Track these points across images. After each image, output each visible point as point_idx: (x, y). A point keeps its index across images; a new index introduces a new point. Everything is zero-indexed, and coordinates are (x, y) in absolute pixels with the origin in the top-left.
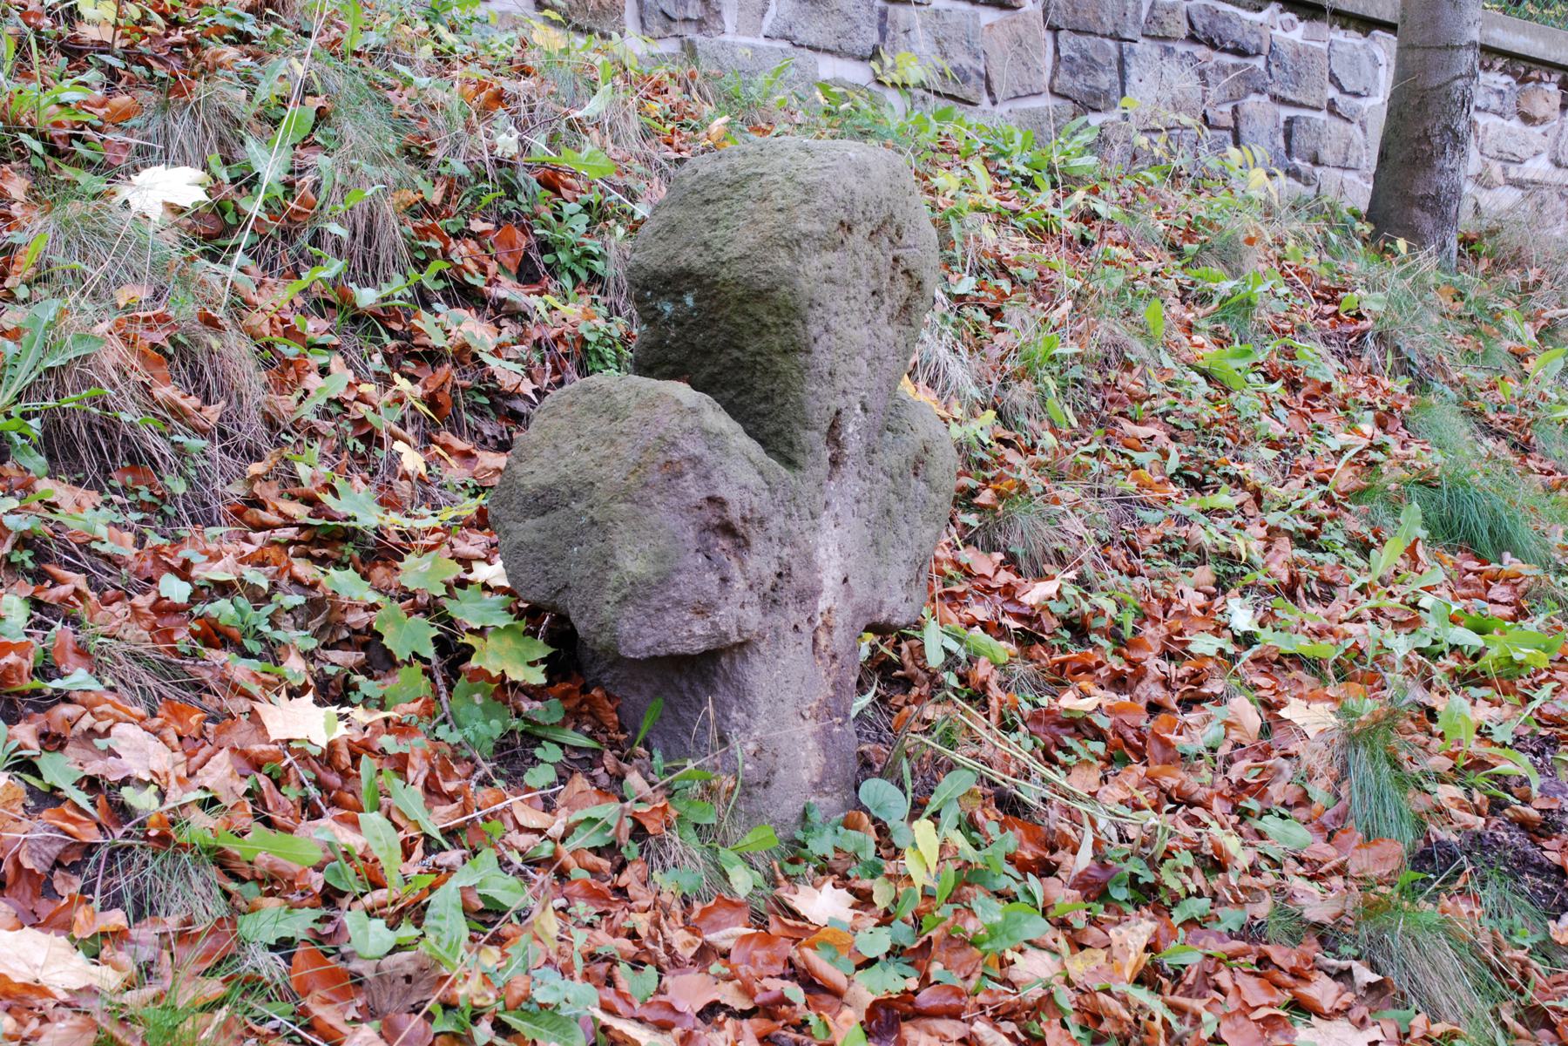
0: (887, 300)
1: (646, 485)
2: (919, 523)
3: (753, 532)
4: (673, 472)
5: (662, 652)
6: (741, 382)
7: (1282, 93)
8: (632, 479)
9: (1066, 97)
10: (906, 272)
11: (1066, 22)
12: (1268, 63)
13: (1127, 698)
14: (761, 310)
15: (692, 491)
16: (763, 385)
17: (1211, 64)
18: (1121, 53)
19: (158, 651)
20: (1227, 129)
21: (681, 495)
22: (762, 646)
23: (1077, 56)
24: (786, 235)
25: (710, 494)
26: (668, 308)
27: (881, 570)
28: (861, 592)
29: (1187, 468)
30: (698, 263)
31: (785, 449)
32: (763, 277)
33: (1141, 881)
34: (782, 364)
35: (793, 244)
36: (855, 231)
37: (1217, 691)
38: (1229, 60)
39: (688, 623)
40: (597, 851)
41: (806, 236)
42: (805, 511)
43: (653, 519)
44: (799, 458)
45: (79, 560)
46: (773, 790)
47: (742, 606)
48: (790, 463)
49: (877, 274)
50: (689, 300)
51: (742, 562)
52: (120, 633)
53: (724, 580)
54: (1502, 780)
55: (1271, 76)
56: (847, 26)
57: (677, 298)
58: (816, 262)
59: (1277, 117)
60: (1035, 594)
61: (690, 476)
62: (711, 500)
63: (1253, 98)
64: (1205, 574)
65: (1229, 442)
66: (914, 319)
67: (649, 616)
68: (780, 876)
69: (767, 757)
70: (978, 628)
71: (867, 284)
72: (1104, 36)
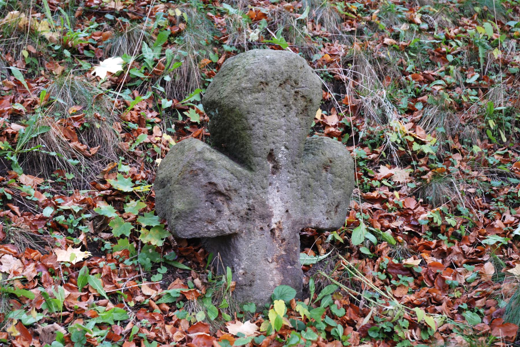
0: (294, 108)
1: (184, 178)
3: (232, 194)
4: (194, 174)
5: (198, 236)
8: (180, 176)
10: (303, 96)
15: (202, 180)
19: (31, 232)
21: (199, 182)
22: (243, 235)
24: (238, 89)
25: (210, 181)
26: (213, 114)
28: (296, 215)
30: (216, 99)
31: (249, 164)
32: (231, 103)
33: (385, 331)
35: (240, 92)
36: (270, 85)
39: (206, 226)
40: (167, 304)
41: (244, 89)
42: (258, 186)
43: (188, 190)
44: (253, 167)
45: (23, 202)
46: (254, 288)
47: (230, 220)
48: (251, 169)
52: (19, 226)
53: (219, 211)
61: (201, 175)
62: (210, 183)
66: (309, 114)
67: (189, 224)
69: (249, 275)
70: (390, 230)
71: (280, 103)
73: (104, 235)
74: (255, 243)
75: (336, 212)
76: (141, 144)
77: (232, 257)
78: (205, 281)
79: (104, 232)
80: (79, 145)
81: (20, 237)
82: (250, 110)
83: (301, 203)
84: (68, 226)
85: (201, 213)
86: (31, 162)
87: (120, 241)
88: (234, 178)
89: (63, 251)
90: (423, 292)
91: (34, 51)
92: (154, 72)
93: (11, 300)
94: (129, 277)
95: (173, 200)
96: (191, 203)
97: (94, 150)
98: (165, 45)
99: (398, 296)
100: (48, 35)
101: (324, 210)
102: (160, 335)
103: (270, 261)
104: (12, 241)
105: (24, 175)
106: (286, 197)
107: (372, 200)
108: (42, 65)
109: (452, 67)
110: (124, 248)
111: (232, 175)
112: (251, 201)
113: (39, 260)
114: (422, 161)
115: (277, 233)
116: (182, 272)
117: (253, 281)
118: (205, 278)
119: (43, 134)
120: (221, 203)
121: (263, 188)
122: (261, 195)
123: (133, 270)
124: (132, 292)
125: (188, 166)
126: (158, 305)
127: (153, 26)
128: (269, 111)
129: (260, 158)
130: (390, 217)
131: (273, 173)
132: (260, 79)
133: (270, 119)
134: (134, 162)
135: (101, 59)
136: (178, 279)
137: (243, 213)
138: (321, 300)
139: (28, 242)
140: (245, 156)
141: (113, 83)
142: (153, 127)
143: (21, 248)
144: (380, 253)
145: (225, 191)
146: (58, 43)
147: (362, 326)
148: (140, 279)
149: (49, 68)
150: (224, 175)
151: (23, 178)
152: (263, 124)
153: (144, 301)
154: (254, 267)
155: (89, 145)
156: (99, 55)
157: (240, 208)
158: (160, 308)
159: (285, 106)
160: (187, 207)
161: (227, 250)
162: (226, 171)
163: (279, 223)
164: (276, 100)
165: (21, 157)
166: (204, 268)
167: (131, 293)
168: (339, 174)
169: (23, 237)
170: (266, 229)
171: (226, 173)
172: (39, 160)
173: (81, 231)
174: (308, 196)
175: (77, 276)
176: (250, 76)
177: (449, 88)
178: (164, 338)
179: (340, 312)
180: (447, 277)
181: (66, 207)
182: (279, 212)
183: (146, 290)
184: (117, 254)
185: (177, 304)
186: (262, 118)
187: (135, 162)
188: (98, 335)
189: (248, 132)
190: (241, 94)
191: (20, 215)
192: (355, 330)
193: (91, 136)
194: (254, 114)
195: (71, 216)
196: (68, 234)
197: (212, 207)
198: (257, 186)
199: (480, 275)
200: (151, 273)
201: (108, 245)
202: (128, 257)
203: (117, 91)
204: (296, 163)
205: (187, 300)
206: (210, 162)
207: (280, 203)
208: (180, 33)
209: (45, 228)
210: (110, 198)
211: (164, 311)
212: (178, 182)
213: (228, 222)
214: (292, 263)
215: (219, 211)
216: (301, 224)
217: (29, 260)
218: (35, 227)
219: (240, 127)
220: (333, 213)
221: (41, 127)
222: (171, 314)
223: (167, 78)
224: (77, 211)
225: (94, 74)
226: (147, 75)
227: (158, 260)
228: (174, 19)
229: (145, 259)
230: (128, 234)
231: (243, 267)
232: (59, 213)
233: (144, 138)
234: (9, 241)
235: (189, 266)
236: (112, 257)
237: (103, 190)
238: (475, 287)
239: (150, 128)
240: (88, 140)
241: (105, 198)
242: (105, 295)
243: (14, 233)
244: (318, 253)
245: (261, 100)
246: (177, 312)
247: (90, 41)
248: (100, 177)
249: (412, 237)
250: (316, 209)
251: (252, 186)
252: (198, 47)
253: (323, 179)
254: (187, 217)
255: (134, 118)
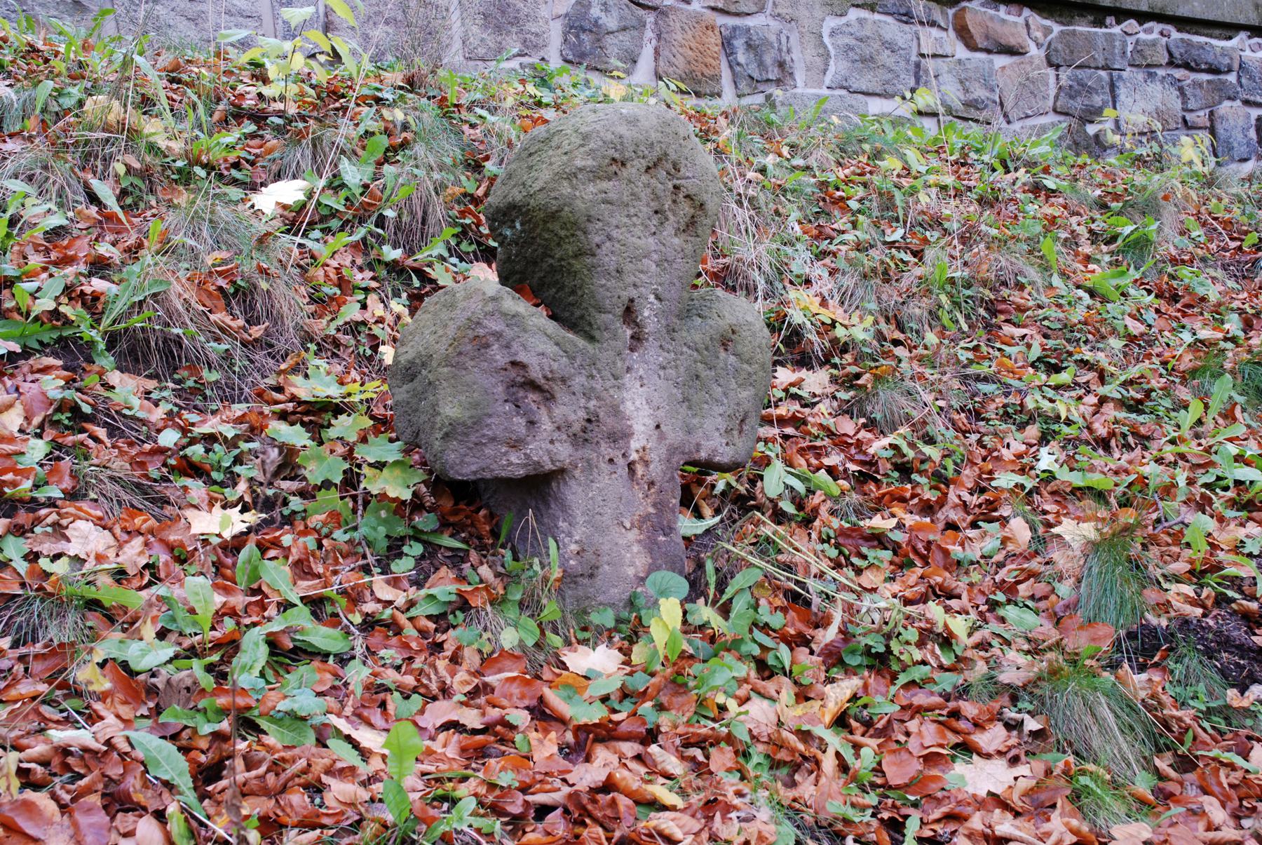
1: (460, 353)
2: (734, 386)
4: (482, 345)
5: (488, 475)
6: (557, 282)
7: (1252, 98)
8: (451, 349)
9: (1067, 114)
10: (687, 196)
11: (1065, 61)
12: (1239, 77)
13: (928, 520)
14: (555, 226)
15: (498, 357)
16: (569, 282)
17: (1188, 82)
18: (1112, 80)
20: (1205, 128)
22: (577, 473)
23: (1075, 84)
26: (508, 233)
27: (695, 421)
28: (674, 435)
29: (1047, 356)
30: (518, 197)
31: (587, 328)
32: (553, 202)
33: (873, 651)
34: (577, 265)
35: (571, 176)
36: (628, 166)
37: (1005, 514)
38: (1205, 77)
39: (505, 454)
40: (429, 617)
41: (580, 170)
42: (606, 373)
43: (469, 378)
44: (597, 334)
46: (598, 581)
47: (552, 442)
48: (591, 339)
49: (657, 198)
50: (518, 225)
51: (550, 410)
53: (532, 423)
54: (1237, 582)
55: (1241, 86)
56: (890, 76)
59: (1248, 116)
61: (496, 347)
62: (514, 363)
63: (1227, 103)
65: (1090, 337)
66: (699, 232)
68: (573, 640)
69: (589, 555)
70: (823, 471)
71: (648, 205)
72: (1097, 68)
73: (286, 485)
74: (600, 490)
75: (741, 432)
76: (346, 323)
77: (555, 518)
78: (500, 569)
79: (284, 479)
80: (228, 320)
81: (110, 487)
82: (592, 213)
83: (683, 410)
84: (212, 466)
85: (496, 426)
86: (132, 351)
87: (321, 495)
88: (562, 353)
89: (203, 513)
90: (913, 575)
91: (137, 165)
93: (89, 614)
94: (346, 566)
95: (438, 400)
96: (476, 405)
97: (257, 331)
98: (379, 164)
99: (869, 587)
100: (162, 143)
101: (723, 427)
102: (425, 681)
103: (628, 525)
104: (93, 495)
105: (118, 373)
106: (656, 399)
107: (782, 421)
109: (861, 217)
110: (330, 508)
112: (592, 404)
113: (151, 531)
114: (848, 357)
115: (640, 470)
116: (450, 554)
117: (597, 568)
118: (499, 563)
119: (155, 295)
120: (534, 406)
121: (616, 378)
122: (612, 392)
123: (351, 551)
124: (354, 594)
125: (469, 328)
126: (410, 619)
127: (355, 134)
128: (626, 220)
129: (610, 316)
130: (815, 448)
131: (632, 350)
132: (612, 152)
133: (628, 236)
134: (334, 355)
135: (263, 185)
136: (444, 570)
137: (576, 427)
138: (730, 600)
139: (126, 497)
140: (578, 313)
143: (111, 509)
144: (815, 511)
145: (543, 381)
146: (180, 157)
147: (826, 645)
148: (366, 570)
149: (167, 198)
150: (541, 348)
151: (115, 377)
152: (617, 246)
153: (382, 613)
154: (597, 538)
155: (247, 321)
157: (572, 417)
158: (415, 627)
159: (656, 212)
160: (468, 414)
161: (541, 507)
162: (545, 339)
163: (644, 449)
164: (639, 199)
165: (112, 340)
166: (493, 546)
167: (354, 597)
168: (747, 356)
169: (118, 488)
170: (621, 462)
171: (545, 343)
172: (149, 348)
173: (239, 476)
174: (695, 398)
175: (234, 564)
176: (592, 145)
177: (859, 247)
178: (434, 687)
179: (777, 620)
180: (950, 547)
181: (206, 429)
182: (643, 428)
183: (385, 592)
184: (316, 520)
185: (451, 617)
186: (615, 233)
187: (337, 356)
188: (1245, 558)
189: (589, 260)
191: (109, 445)
192: (812, 652)
194: (600, 224)
195: (216, 447)
196: (211, 482)
197: (518, 413)
198: (604, 373)
199: (1005, 541)
200: (388, 557)
201: (296, 503)
202: (340, 527)
203: (296, 234)
204: (674, 331)
205: (471, 607)
206: (513, 319)
207: (646, 411)
208: (404, 145)
209: (164, 470)
210: (293, 418)
211: (423, 633)
212: (447, 361)
213: (550, 447)
214: (667, 531)
215: (532, 423)
216: (683, 453)
217: (129, 533)
218: (142, 465)
219: (570, 249)
220: (735, 433)
222: (440, 637)
223: (390, 213)
224: (230, 436)
225: (253, 206)
227: (401, 530)
228: (391, 126)
229: (375, 529)
230: (337, 479)
231: (577, 538)
232: (193, 441)
233: (351, 312)
234: (86, 495)
235: (464, 541)
236: (306, 527)
237: (277, 402)
238: (1001, 565)
239: (361, 297)
241: (283, 416)
242: (298, 602)
243: (96, 478)
244: (699, 515)
245: (612, 196)
246: (451, 632)
247: (243, 154)
248: (271, 381)
249: (864, 482)
250: (709, 424)
251: (595, 372)
252: (442, 167)
253: (721, 365)
254: (466, 435)
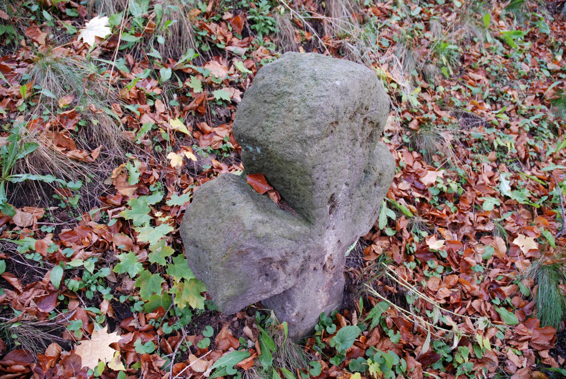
1: (230, 261)
15: (254, 258)
24: (299, 137)
25: (264, 257)
32: (287, 155)
36: (340, 123)
41: (309, 138)
43: (237, 270)
44: (312, 220)
57: (254, 147)
58: (316, 147)
60: (429, 178)
64: (493, 155)
92: (147, 32)
108: (20, 32)
111: (290, 241)
141: (103, 49)
142: (154, 103)
156: (84, 13)
176: (318, 119)
190: (305, 145)
193: (89, 133)
221: (26, 145)
226: (140, 35)
239: (151, 103)
240: (88, 139)
255: (133, 95)
